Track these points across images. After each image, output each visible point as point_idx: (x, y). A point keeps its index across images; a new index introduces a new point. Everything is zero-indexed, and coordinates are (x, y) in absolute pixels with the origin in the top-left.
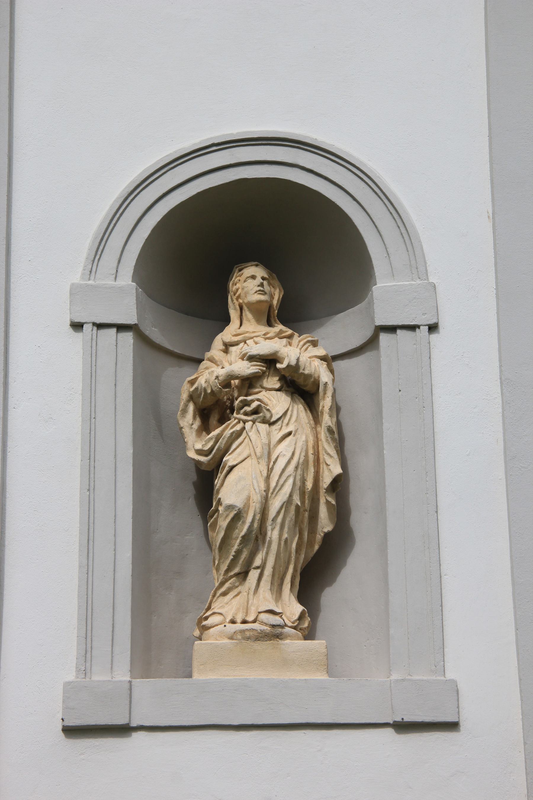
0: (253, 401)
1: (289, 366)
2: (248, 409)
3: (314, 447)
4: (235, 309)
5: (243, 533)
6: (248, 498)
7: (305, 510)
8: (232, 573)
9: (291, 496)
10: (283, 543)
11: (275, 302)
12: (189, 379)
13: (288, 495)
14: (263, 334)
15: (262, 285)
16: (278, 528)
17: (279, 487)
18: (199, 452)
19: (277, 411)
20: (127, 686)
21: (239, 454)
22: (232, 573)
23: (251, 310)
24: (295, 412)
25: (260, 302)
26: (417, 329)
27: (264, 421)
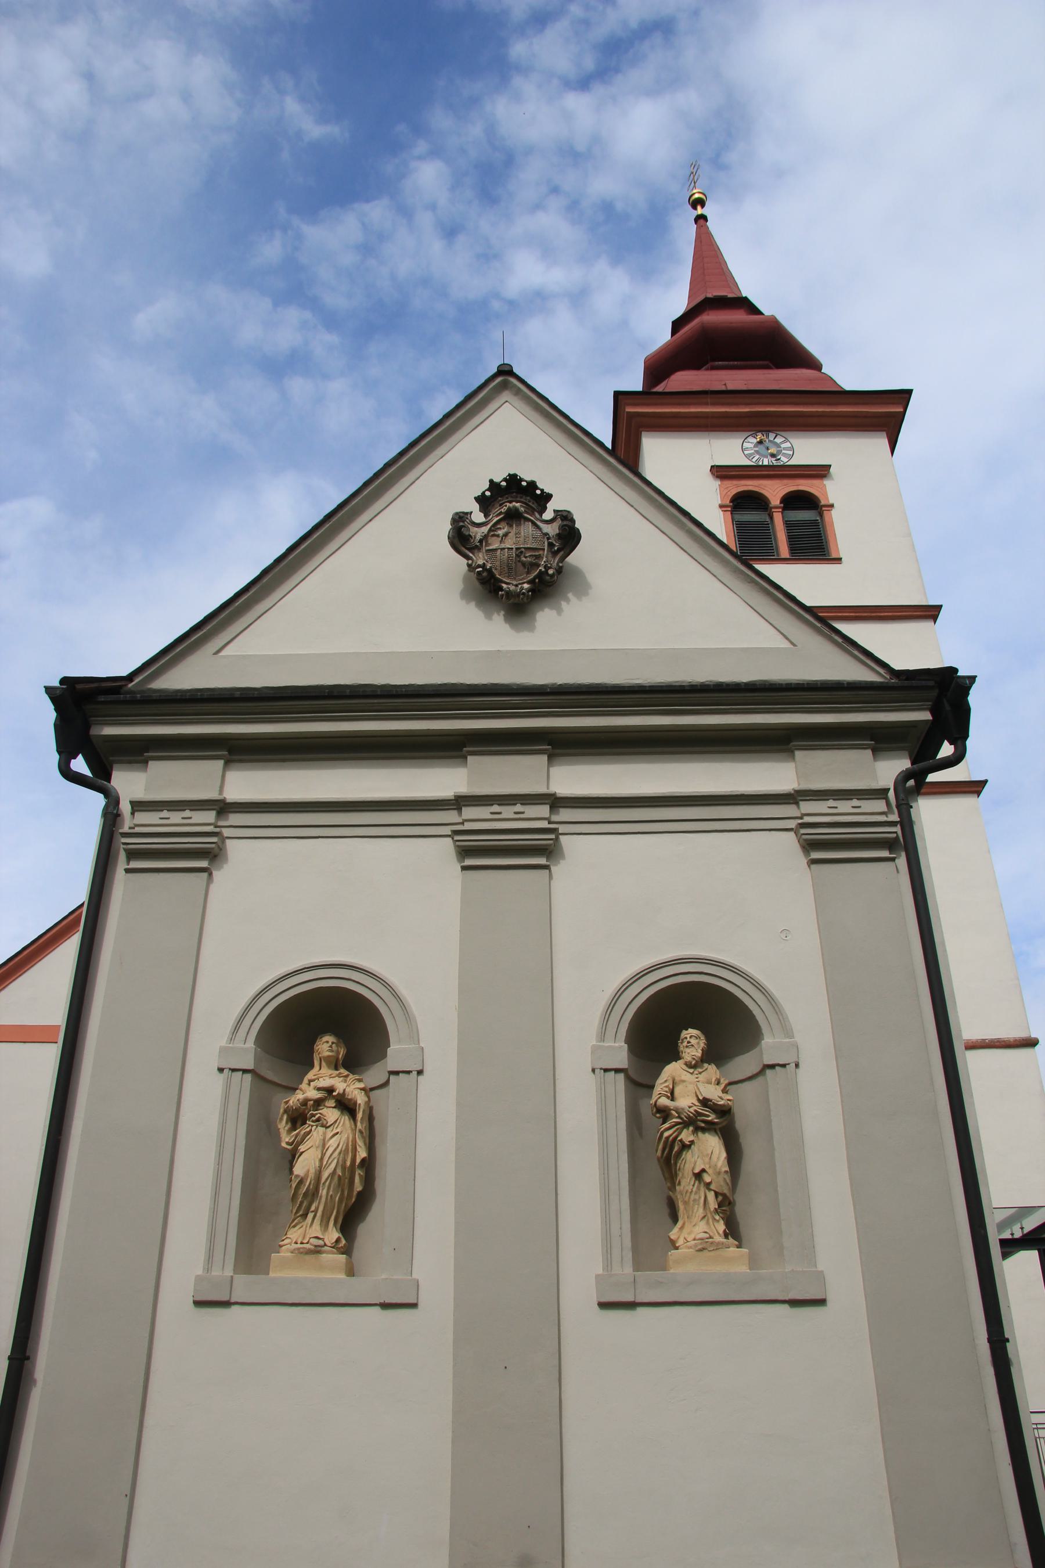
0: (317, 1114)
1: (338, 1094)
2: (314, 1118)
3: (352, 1141)
4: (317, 1060)
5: (303, 1192)
6: (308, 1171)
7: (346, 1178)
8: (298, 1215)
9: (335, 1169)
10: (329, 1197)
11: (340, 1056)
12: (285, 1100)
13: (333, 1169)
15: (331, 1046)
16: (326, 1188)
17: (328, 1165)
18: (288, 1143)
19: (331, 1121)
20: (230, 1278)
21: (307, 1145)
22: (298, 1215)
23: (325, 1062)
24: (342, 1120)
25: (329, 1056)
27: (323, 1126)
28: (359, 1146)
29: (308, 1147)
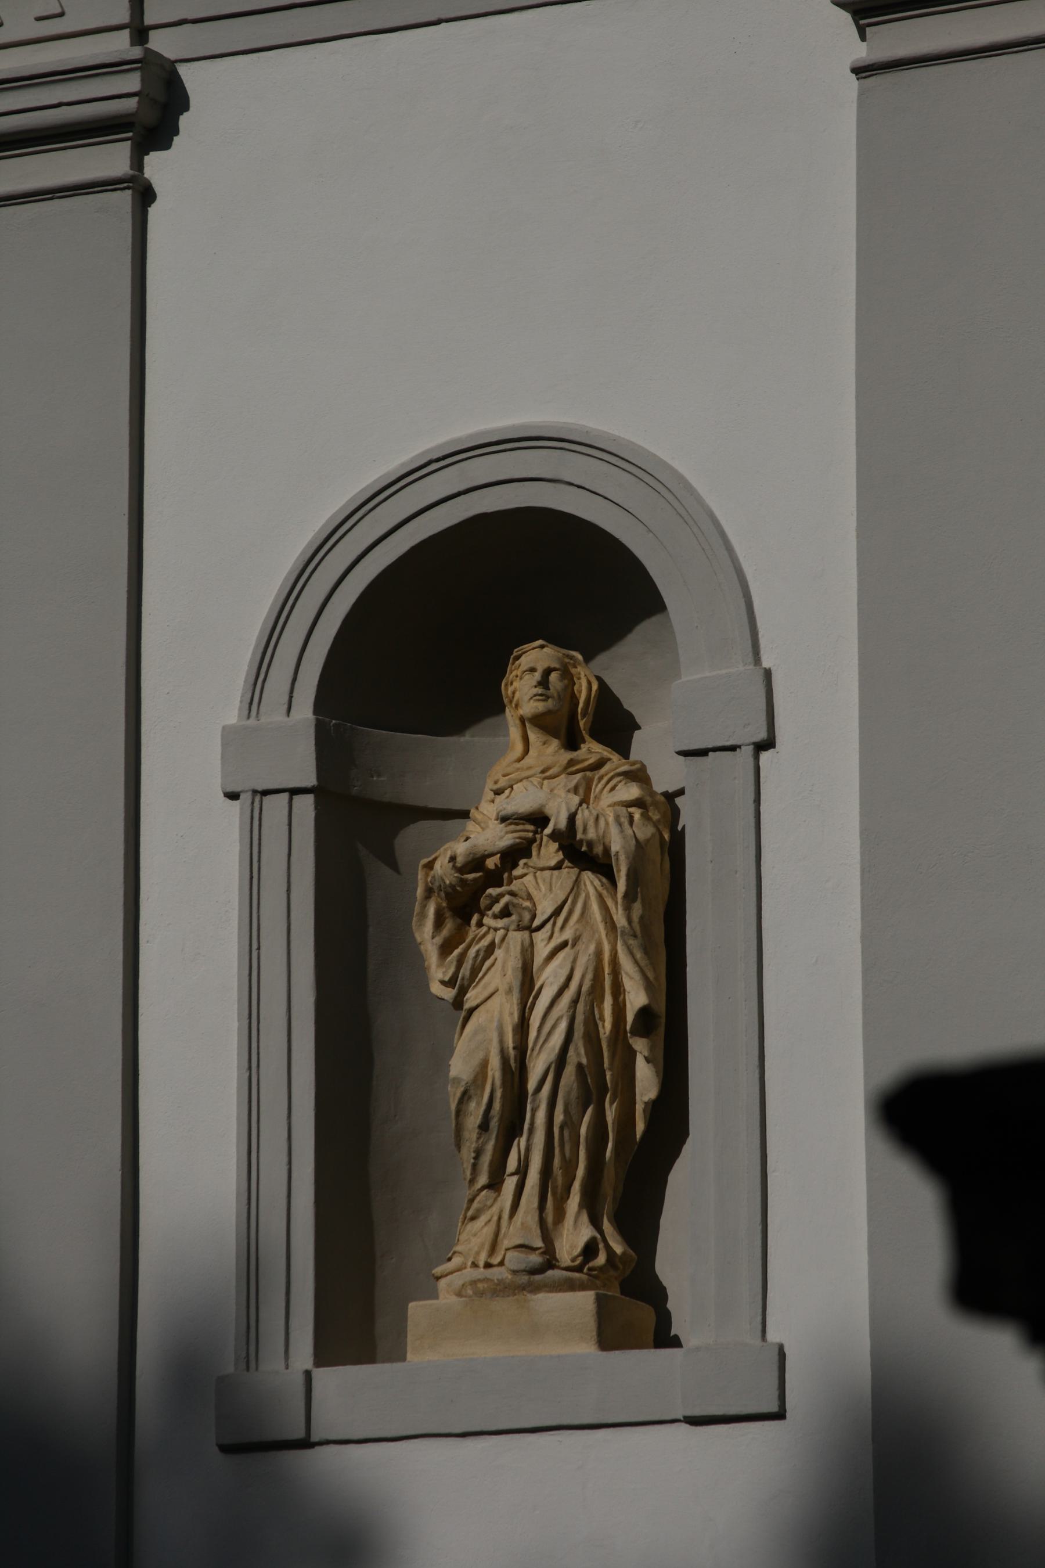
2: (497, 908)
6: (484, 1064)
14: (539, 771)
21: (485, 987)
26: (738, 749)
28: (627, 974)
29: (486, 994)
